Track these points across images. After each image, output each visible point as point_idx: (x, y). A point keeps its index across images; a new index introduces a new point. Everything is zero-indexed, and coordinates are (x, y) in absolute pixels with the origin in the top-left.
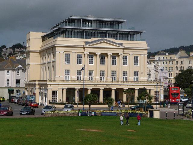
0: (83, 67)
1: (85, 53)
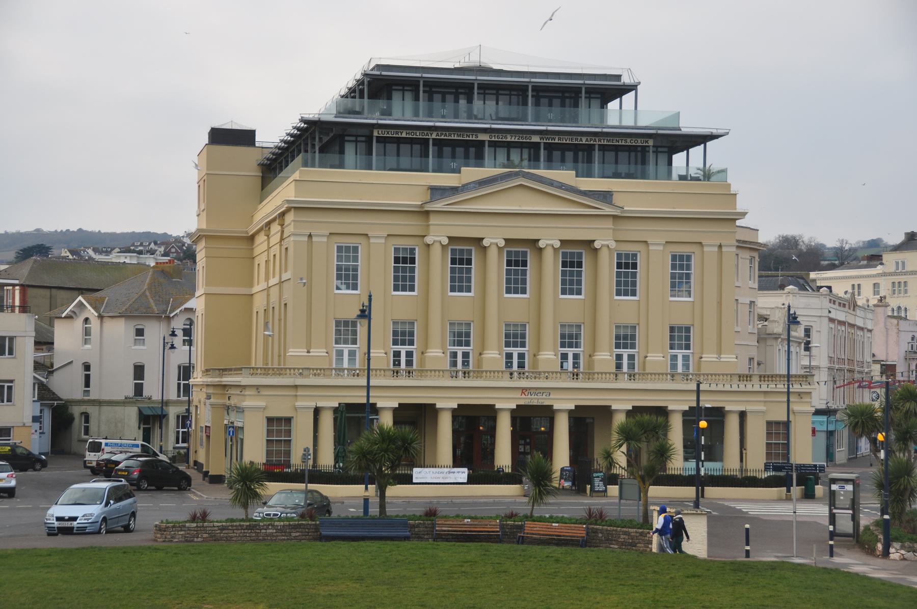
0: (366, 304)
1: (429, 240)
